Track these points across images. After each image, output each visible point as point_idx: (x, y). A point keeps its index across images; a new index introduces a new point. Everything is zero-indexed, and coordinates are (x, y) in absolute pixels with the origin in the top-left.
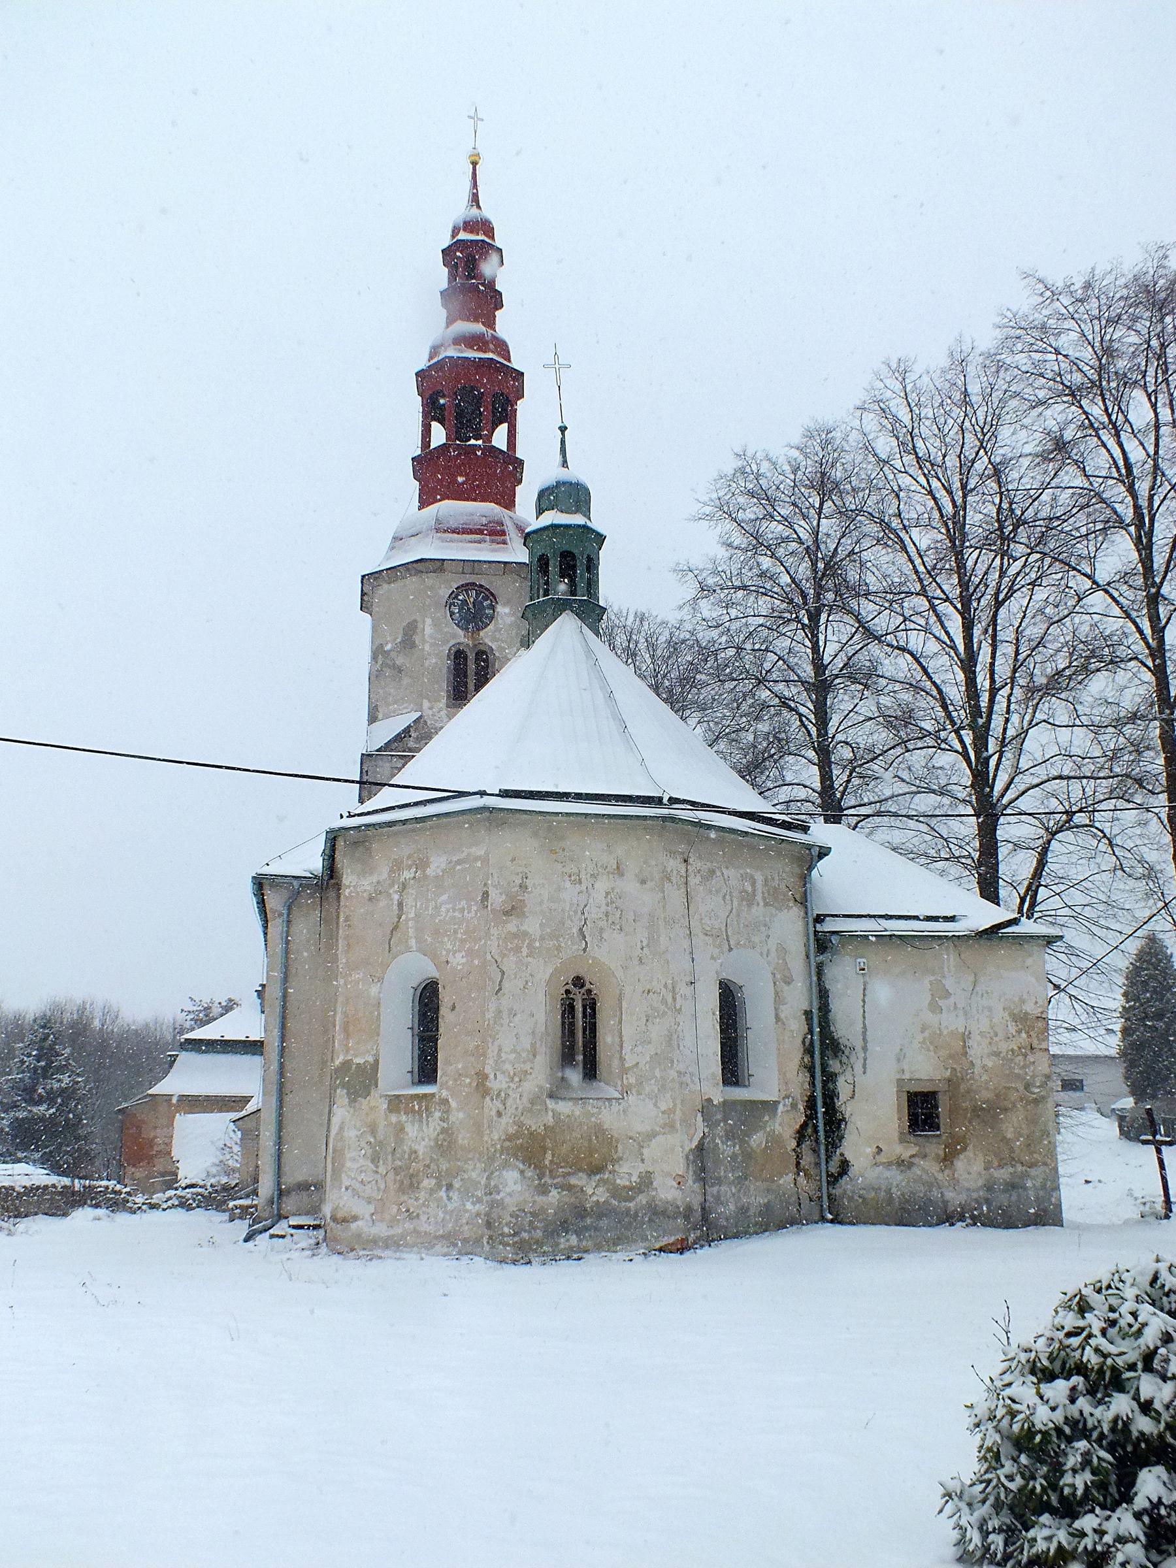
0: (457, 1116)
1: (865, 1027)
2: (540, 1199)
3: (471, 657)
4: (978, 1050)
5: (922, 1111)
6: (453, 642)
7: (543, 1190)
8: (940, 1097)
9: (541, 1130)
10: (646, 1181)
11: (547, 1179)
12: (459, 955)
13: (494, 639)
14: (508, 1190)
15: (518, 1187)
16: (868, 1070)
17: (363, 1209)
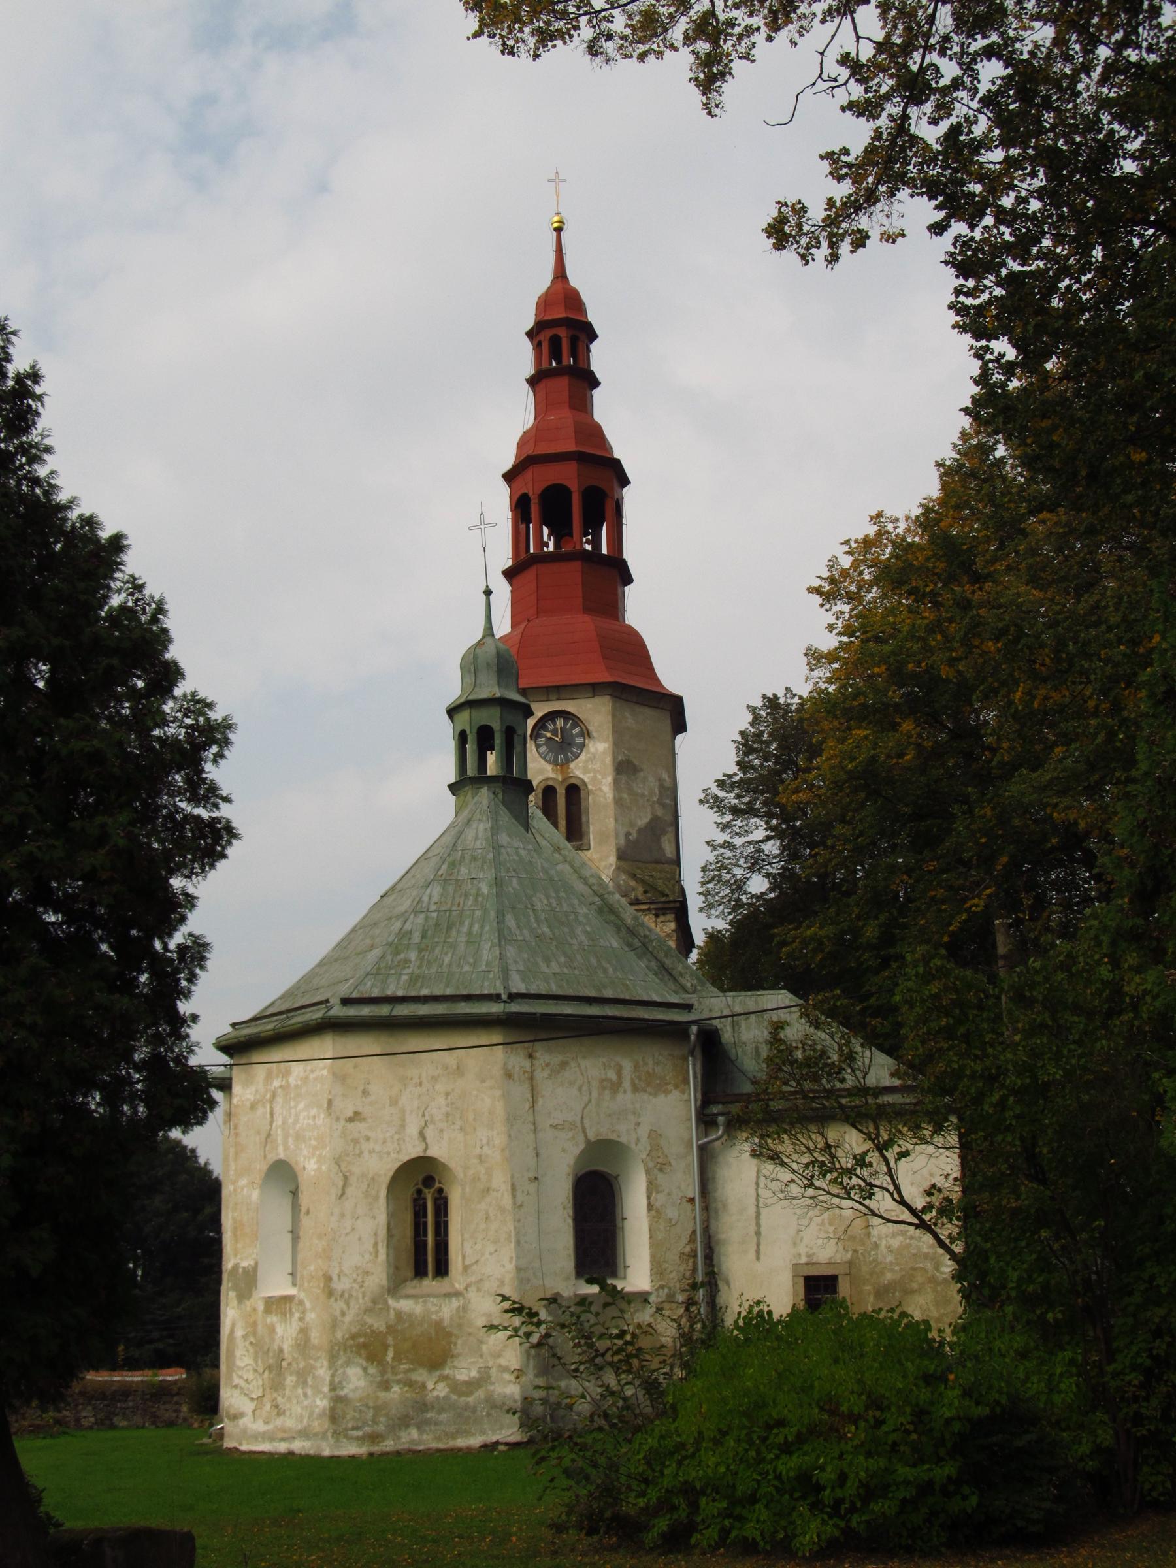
0: (311, 1316)
2: (382, 1394)
3: (561, 792)
7: (385, 1386)
8: (840, 1278)
9: (383, 1328)
10: (483, 1379)
11: (389, 1375)
12: (313, 1161)
13: (586, 770)
14: (351, 1386)
15: (362, 1383)
16: (762, 1256)
17: (247, 1407)
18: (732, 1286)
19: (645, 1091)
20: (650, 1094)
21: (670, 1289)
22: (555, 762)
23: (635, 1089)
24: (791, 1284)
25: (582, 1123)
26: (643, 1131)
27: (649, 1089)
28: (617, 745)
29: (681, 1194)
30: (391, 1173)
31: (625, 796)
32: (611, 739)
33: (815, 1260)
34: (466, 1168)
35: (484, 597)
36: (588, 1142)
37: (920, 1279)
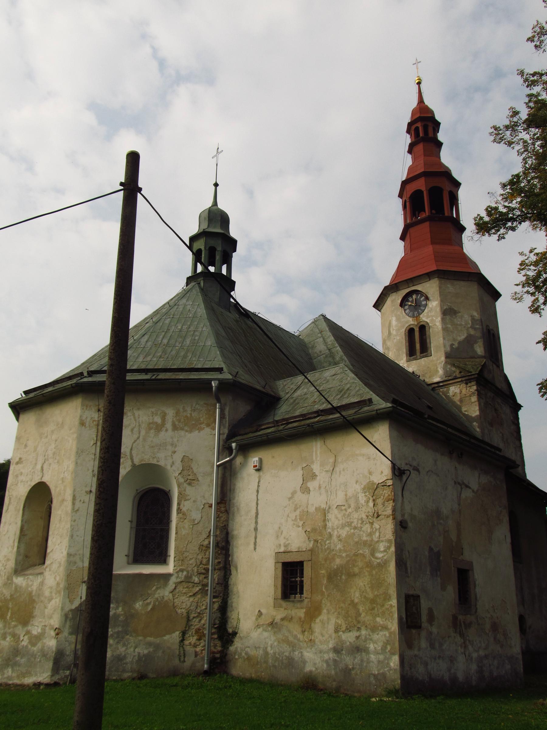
1: (257, 514)
3: (417, 330)
4: (335, 519)
5: (292, 577)
6: (407, 325)
13: (428, 317)
16: (257, 547)
18: (239, 571)
19: (182, 429)
20: (187, 431)
21: (188, 572)
22: (413, 316)
23: (175, 428)
24: (274, 568)
25: (131, 453)
26: (178, 458)
27: (186, 428)
28: (443, 301)
29: (204, 501)
30: (26, 495)
31: (449, 326)
32: (439, 298)
33: (289, 549)
34: (56, 487)
35: (214, 187)
36: (134, 466)
37: (360, 564)
